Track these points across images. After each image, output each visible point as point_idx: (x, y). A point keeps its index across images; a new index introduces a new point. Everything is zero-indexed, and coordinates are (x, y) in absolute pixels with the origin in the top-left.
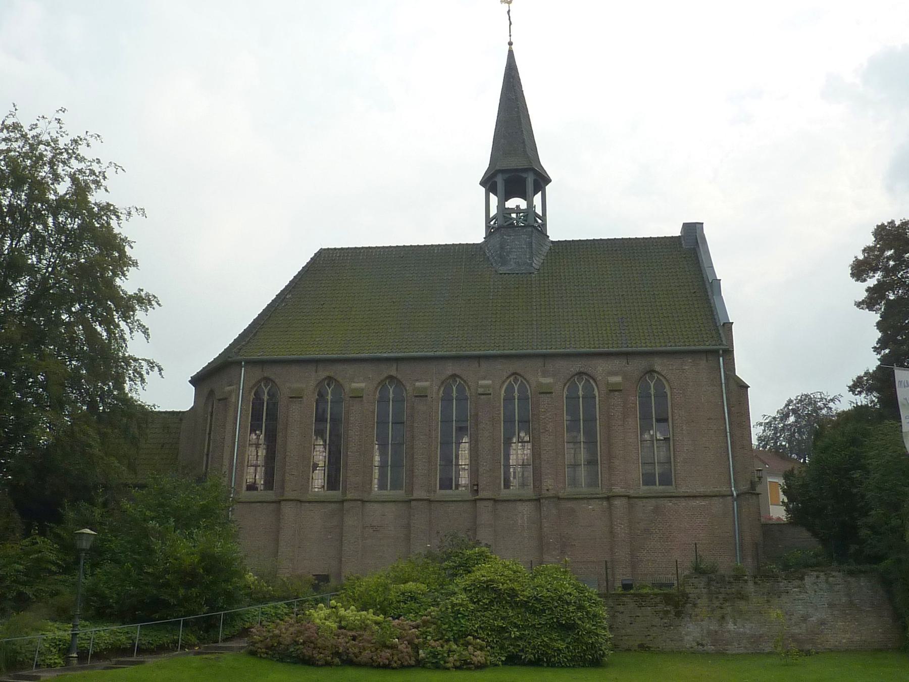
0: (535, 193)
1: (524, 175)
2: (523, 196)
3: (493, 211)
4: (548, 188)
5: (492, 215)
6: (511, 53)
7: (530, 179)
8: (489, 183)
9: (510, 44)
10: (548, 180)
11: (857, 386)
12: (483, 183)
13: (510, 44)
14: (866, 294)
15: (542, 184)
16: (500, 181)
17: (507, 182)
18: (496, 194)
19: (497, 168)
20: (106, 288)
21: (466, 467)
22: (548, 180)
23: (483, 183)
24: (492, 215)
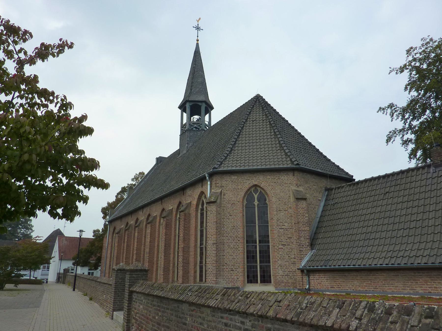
0: (206, 114)
1: (200, 104)
2: (199, 114)
3: (185, 121)
4: (212, 112)
5: (184, 123)
6: (197, 44)
7: (203, 106)
8: (182, 107)
9: (198, 40)
10: (212, 108)
11: (133, 180)
12: (180, 107)
13: (198, 40)
14: (107, 205)
15: (209, 109)
16: (188, 106)
17: (192, 108)
18: (186, 113)
19: (187, 99)
20: (390, 314)
21: (32, 273)
22: (212, 108)
23: (180, 107)
24: (184, 123)
